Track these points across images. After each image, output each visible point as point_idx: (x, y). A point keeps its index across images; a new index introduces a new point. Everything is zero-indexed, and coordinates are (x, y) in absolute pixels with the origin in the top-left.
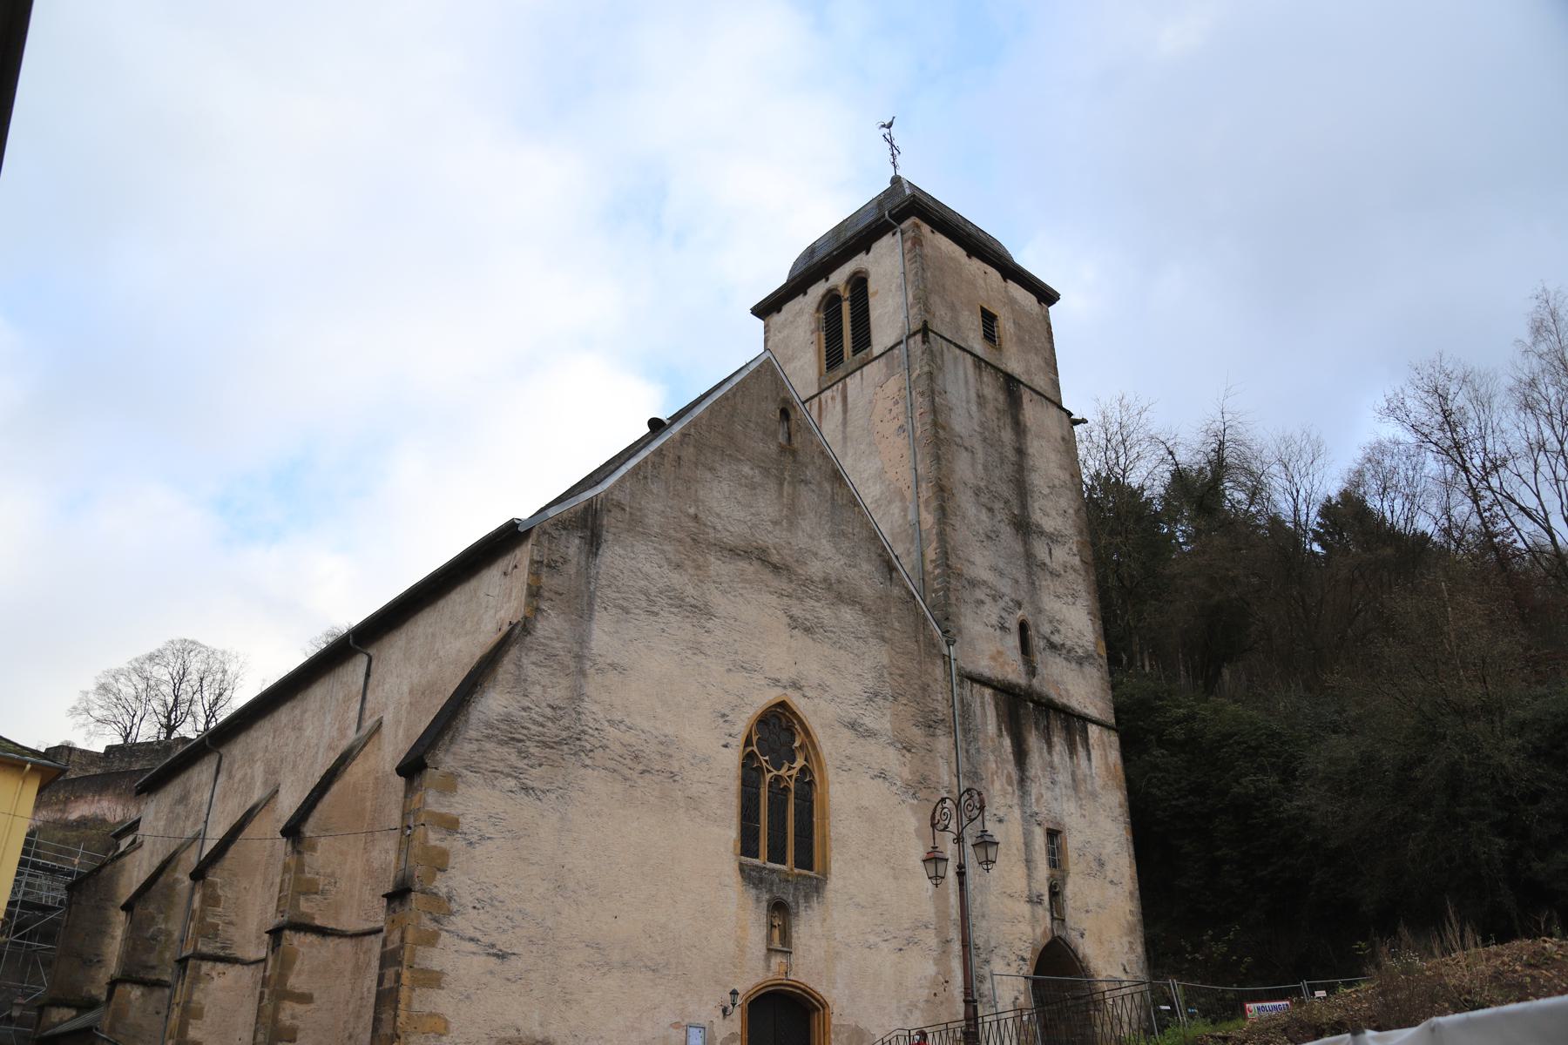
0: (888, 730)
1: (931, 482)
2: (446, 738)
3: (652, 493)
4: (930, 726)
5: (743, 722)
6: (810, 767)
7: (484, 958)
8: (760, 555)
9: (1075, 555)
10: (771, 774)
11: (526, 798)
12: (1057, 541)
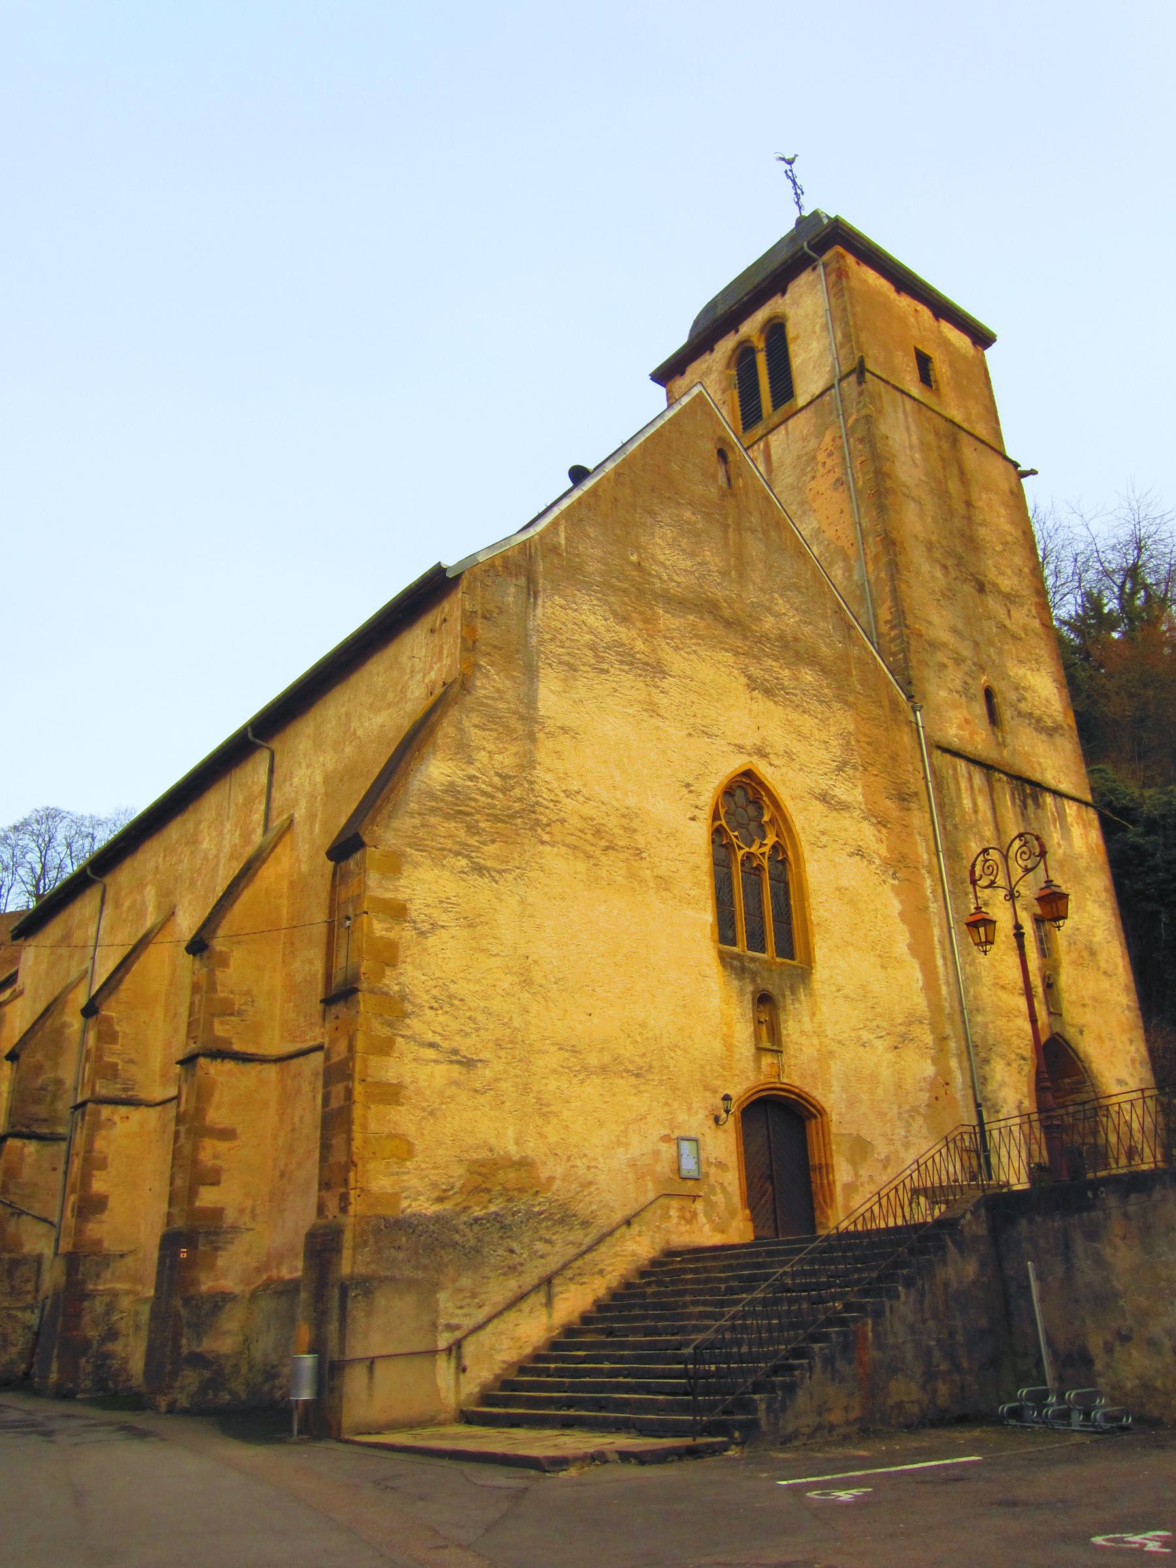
0: (860, 803)
1: (880, 535)
2: (384, 811)
3: (588, 537)
4: (904, 799)
5: (709, 792)
6: (783, 843)
8: (709, 608)
9: (1034, 617)
10: (743, 852)
11: (480, 879)
12: (1015, 602)
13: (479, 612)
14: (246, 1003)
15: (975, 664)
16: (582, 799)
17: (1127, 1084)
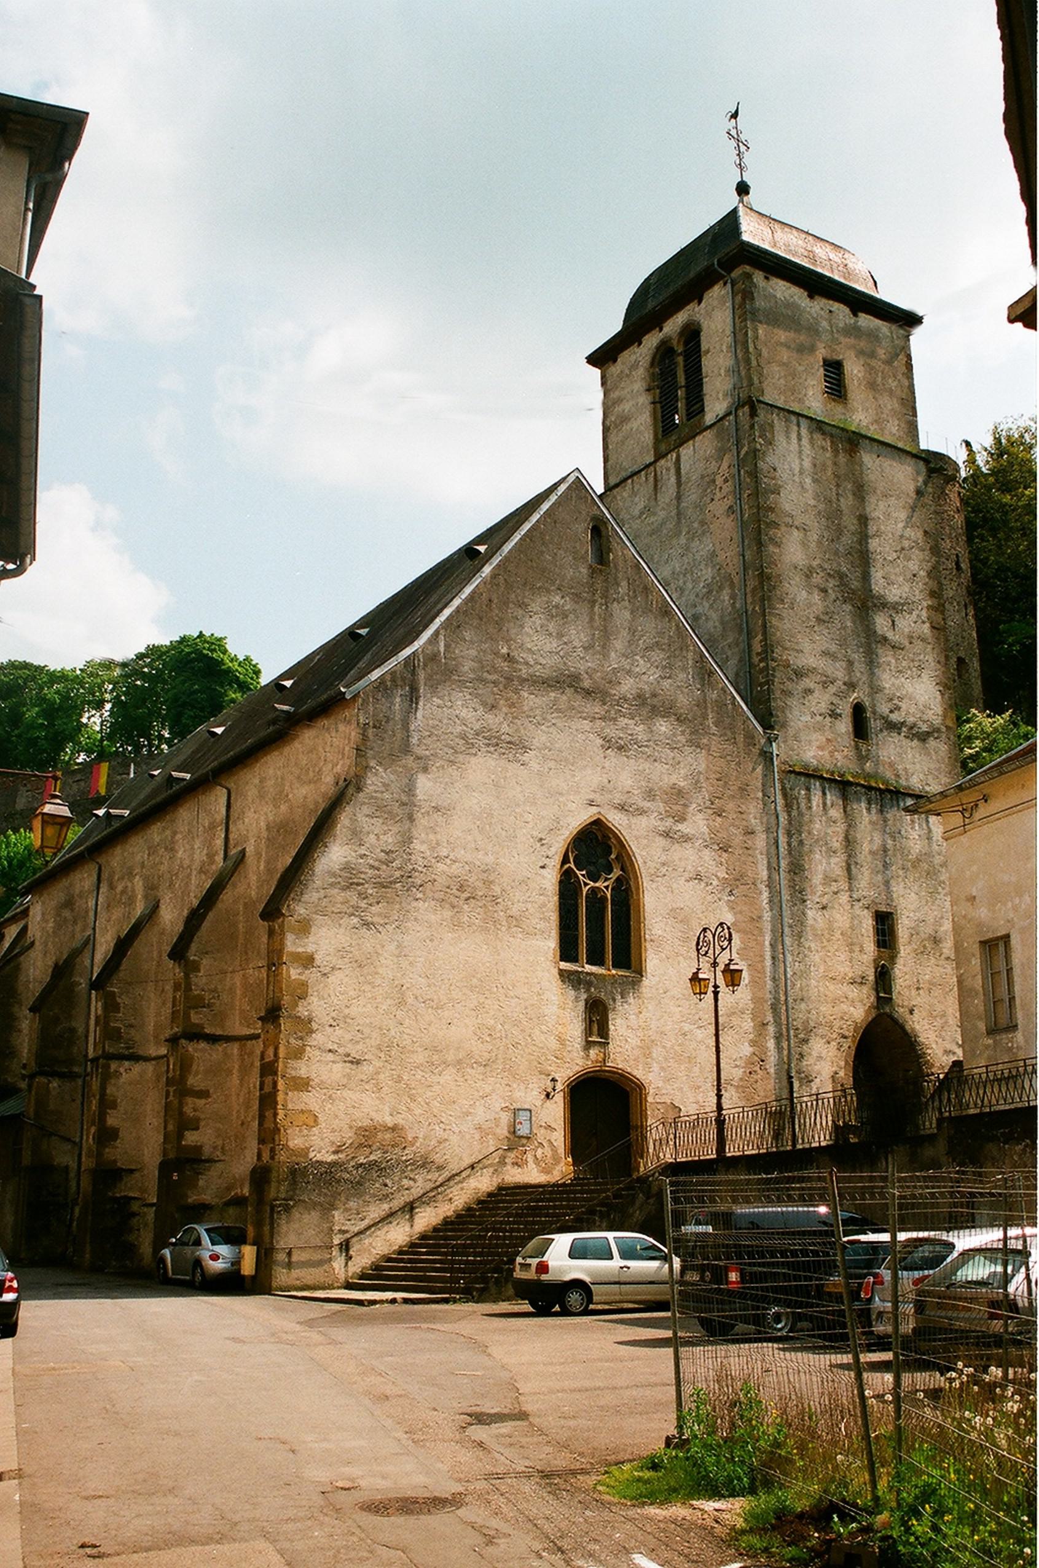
5: (559, 844)
7: (341, 1065)
10: (588, 887)
13: (371, 724)
14: (214, 997)
15: (845, 684)
16: (449, 862)
17: (954, 1053)
